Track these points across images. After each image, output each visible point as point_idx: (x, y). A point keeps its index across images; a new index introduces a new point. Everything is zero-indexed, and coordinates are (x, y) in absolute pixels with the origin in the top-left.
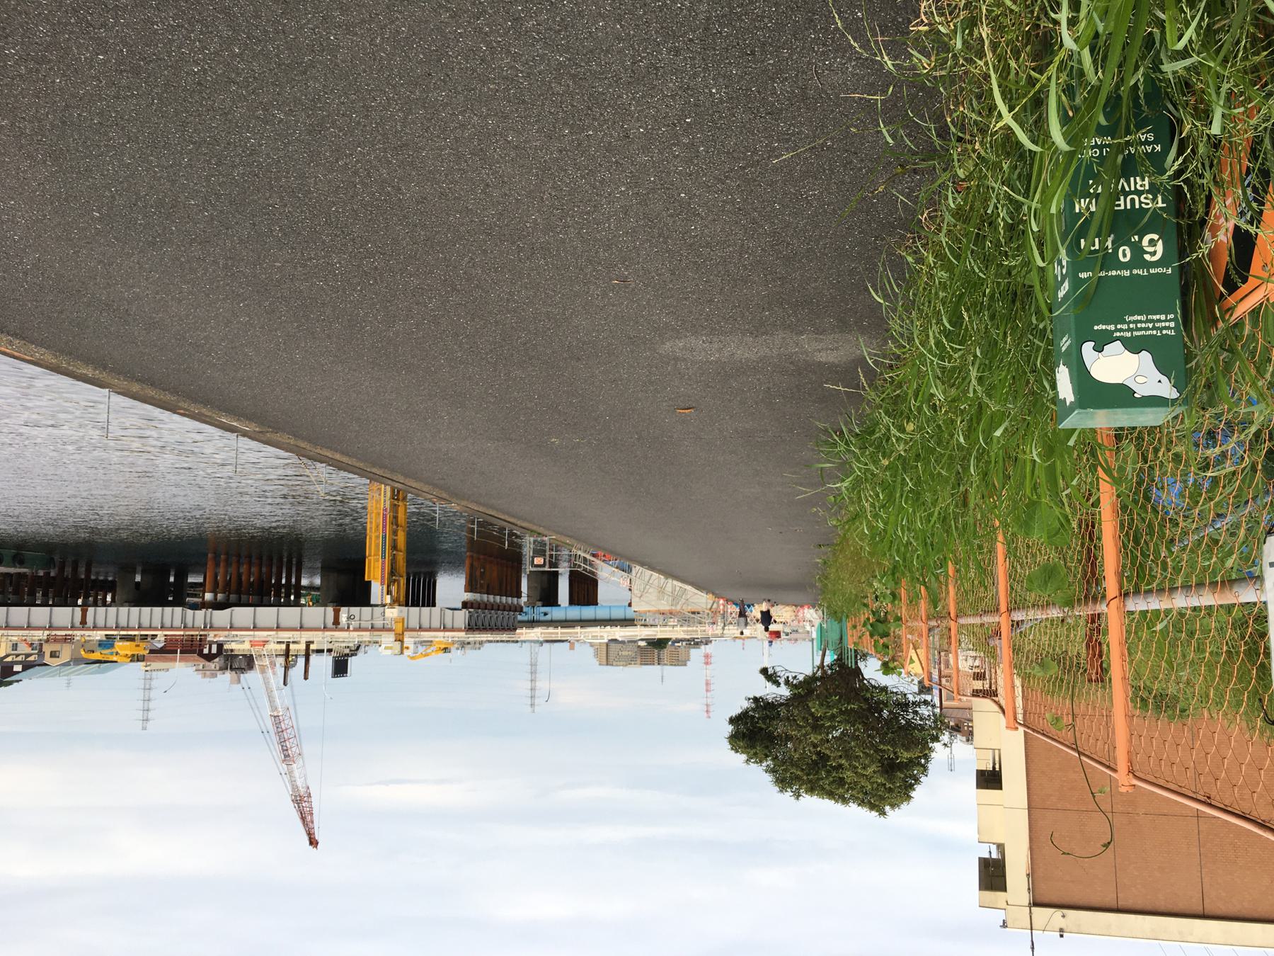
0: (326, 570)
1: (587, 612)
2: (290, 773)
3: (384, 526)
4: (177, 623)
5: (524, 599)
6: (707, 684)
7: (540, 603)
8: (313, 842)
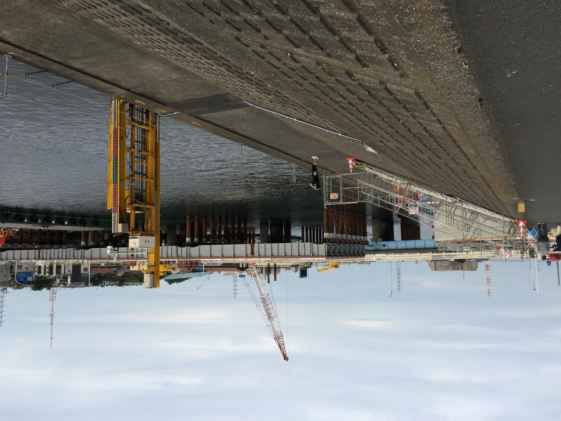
1: (411, 244)
2: (272, 325)
4: (174, 255)
5: (369, 238)
6: (488, 279)
7: (380, 239)
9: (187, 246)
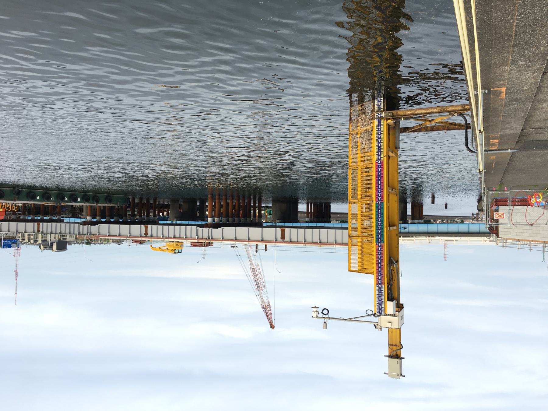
0: (274, 201)
2: (261, 294)
4: (194, 235)
7: (401, 222)
8: (272, 327)
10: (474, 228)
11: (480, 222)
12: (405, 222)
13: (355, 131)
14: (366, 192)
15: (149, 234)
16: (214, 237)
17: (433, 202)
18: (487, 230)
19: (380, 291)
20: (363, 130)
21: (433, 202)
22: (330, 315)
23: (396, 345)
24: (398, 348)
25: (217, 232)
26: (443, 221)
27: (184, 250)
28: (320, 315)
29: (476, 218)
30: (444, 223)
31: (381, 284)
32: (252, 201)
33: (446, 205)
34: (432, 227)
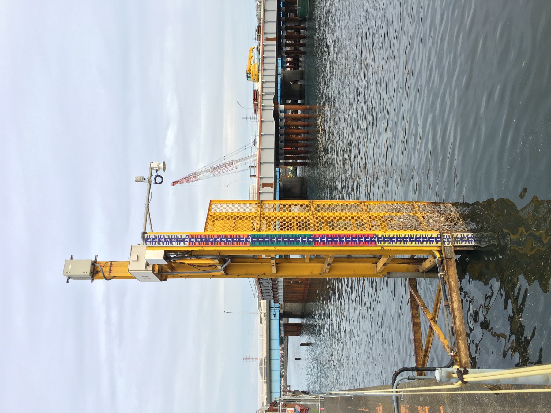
0: (303, 180)
2: (206, 171)
3: (330, 240)
4: (266, 91)
7: (282, 312)
9: (274, 107)
10: (277, 387)
11: (282, 393)
12: (282, 316)
13: (417, 209)
14: (327, 222)
15: (266, 43)
16: (264, 112)
17: (302, 344)
18: (273, 401)
19: (179, 240)
20: (421, 219)
21: (302, 344)
22: (154, 186)
23: (110, 271)
24: (107, 275)
25: (269, 115)
26: (283, 357)
27: (251, 83)
28: (154, 173)
29: (286, 389)
30: (280, 358)
31: (190, 241)
32: (301, 161)
33: (299, 359)
34: (276, 344)
